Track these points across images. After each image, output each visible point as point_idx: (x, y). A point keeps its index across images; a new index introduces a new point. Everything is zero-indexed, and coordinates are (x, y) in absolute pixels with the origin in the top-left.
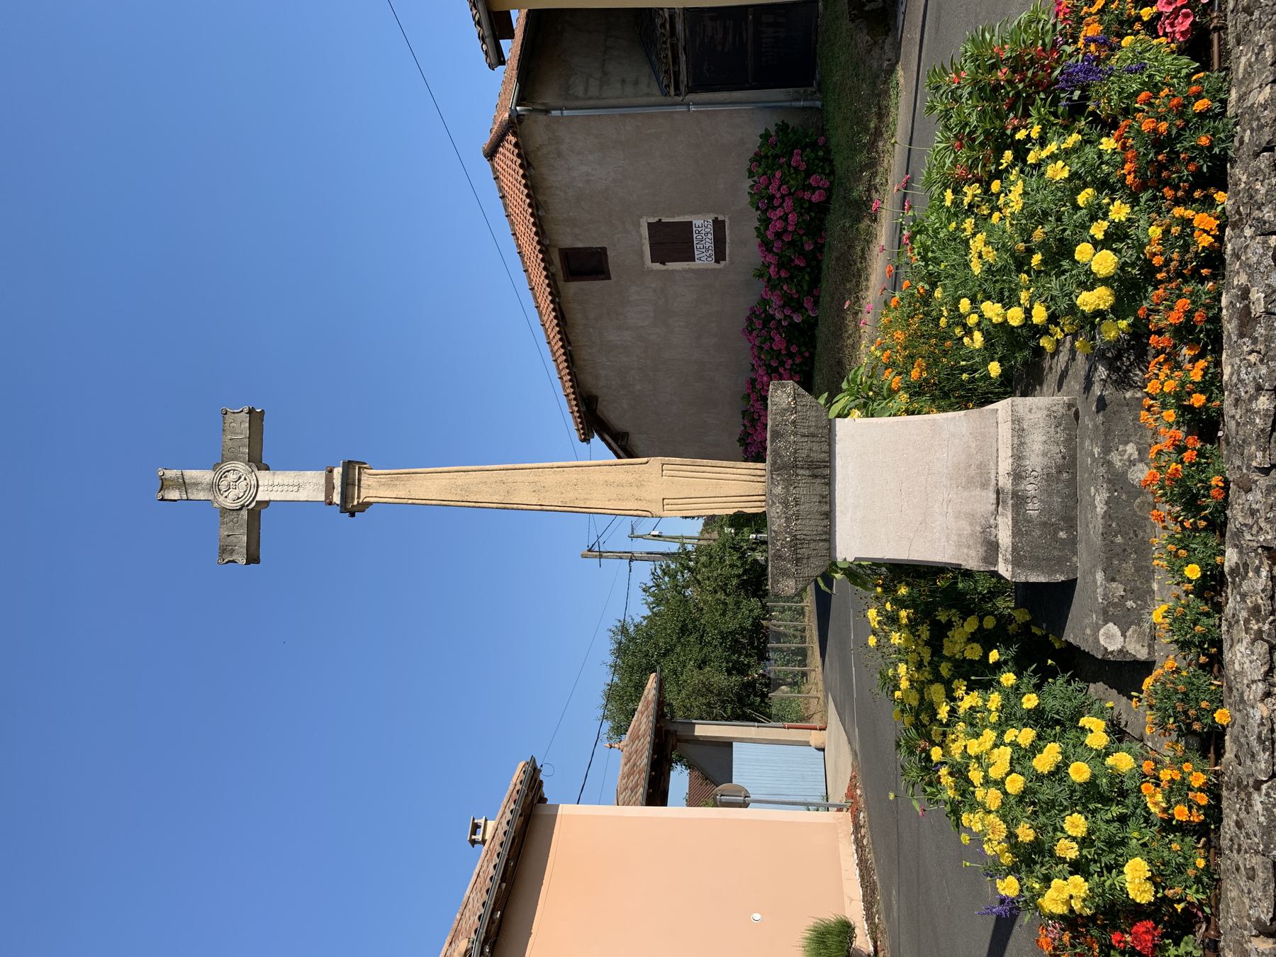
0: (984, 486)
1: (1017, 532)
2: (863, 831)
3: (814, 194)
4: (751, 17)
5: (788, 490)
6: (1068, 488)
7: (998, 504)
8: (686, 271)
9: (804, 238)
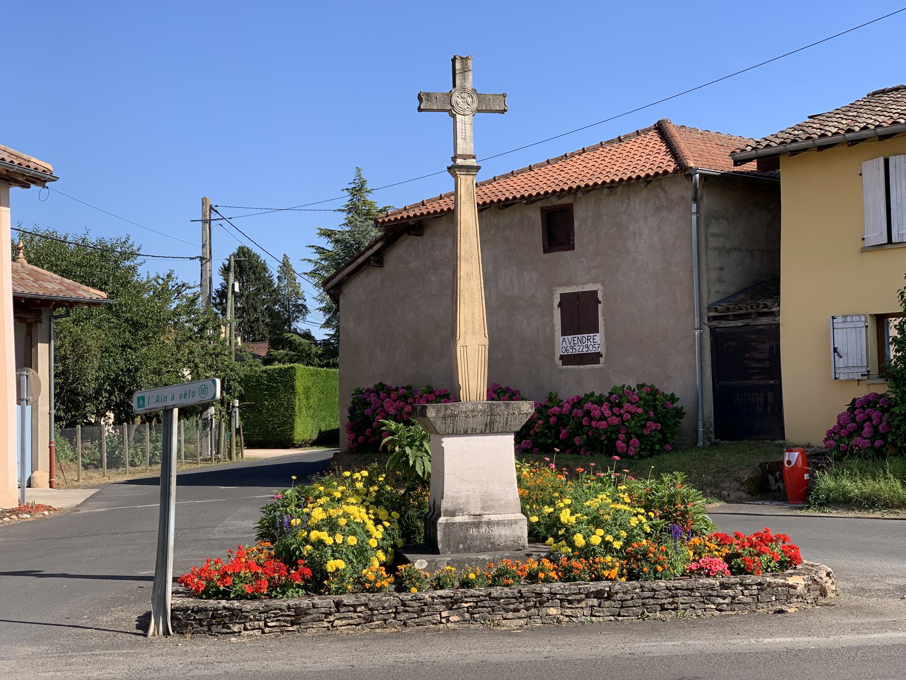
0: (483, 508)
1: (462, 524)
2: (14, 517)
3: (623, 442)
4: (772, 382)
8: (553, 326)
9: (585, 436)
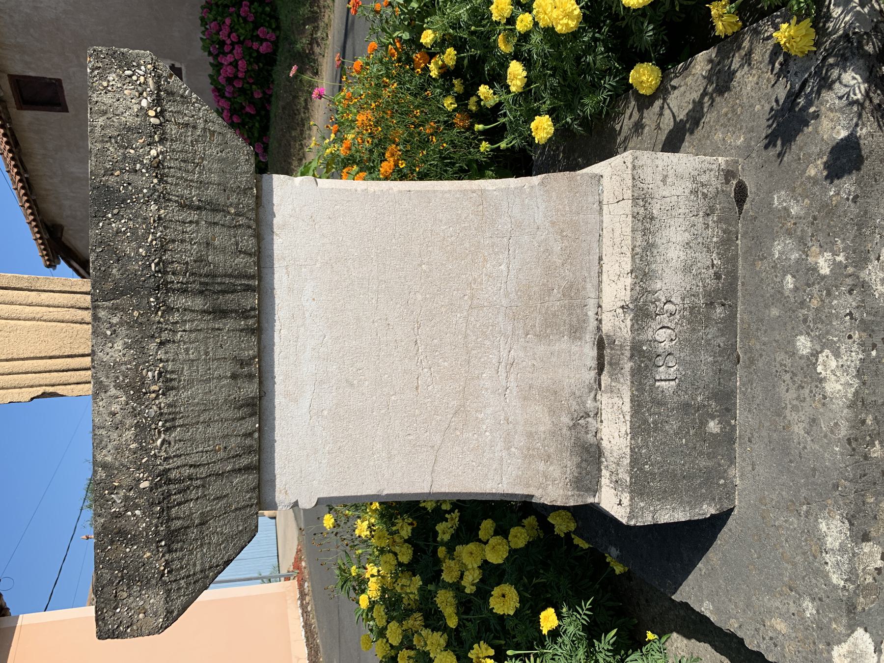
0: (576, 332)
2: (307, 598)
5: (143, 350)
6: (722, 335)
7: (600, 369)
9: (254, 87)
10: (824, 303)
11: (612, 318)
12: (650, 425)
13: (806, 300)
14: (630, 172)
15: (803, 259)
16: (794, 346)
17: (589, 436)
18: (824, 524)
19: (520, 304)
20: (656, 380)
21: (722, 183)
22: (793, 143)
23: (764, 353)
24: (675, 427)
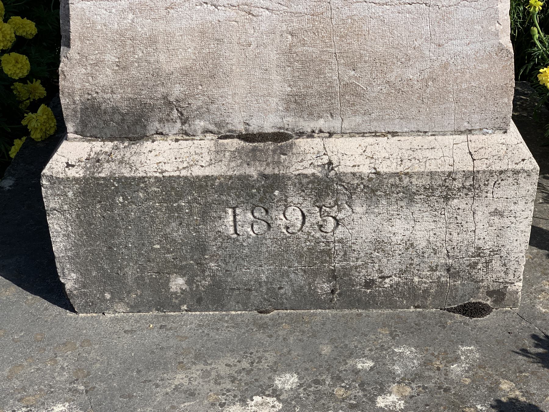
6: (294, 292)
7: (247, 137)
10: (341, 402)
11: (315, 150)
12: (176, 202)
13: (343, 382)
14: (510, 167)
15: (394, 378)
16: (285, 371)
17: (157, 124)
18: (63, 408)
19: (334, 23)
20: (234, 209)
21: (488, 287)
22: (540, 365)
23: (273, 339)
24: (175, 234)
